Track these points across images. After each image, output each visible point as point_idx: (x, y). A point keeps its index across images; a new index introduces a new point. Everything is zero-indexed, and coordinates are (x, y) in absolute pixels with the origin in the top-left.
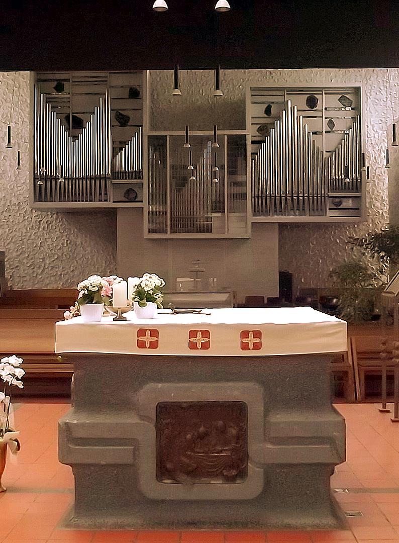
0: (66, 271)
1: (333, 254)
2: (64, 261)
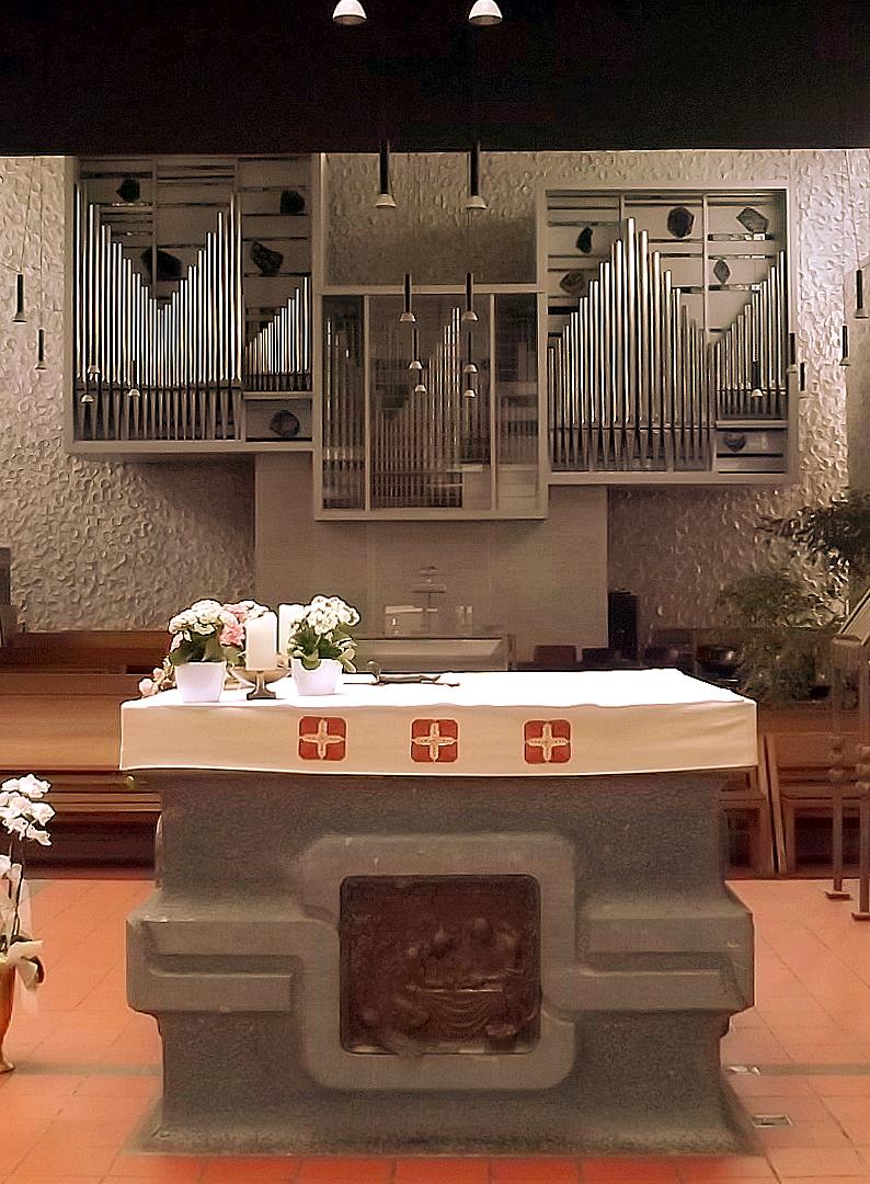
0: (144, 591)
1: (726, 554)
2: (140, 568)
